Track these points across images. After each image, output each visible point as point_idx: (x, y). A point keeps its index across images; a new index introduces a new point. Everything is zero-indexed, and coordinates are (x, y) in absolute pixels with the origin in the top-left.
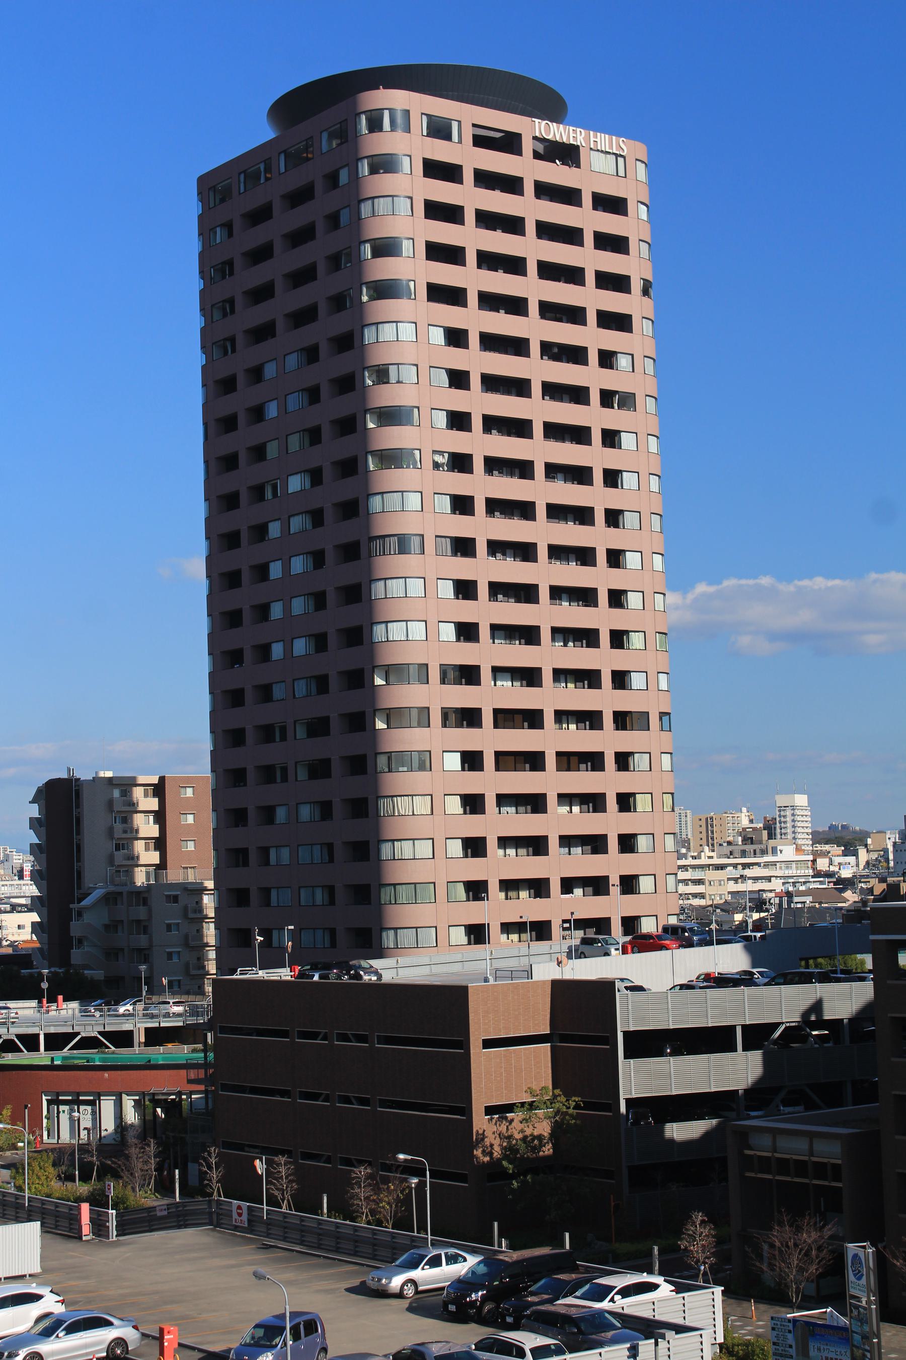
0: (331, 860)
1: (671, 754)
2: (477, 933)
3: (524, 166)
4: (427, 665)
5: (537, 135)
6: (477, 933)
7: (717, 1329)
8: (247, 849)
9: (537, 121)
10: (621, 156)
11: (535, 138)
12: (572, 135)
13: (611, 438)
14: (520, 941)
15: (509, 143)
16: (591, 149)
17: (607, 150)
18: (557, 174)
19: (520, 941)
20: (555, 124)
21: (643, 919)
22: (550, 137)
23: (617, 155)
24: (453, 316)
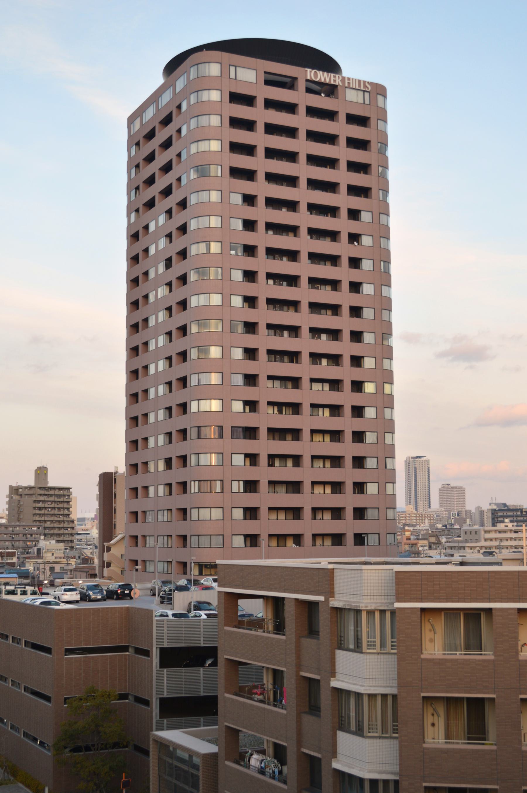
0: (171, 494)
1: (378, 483)
2: (252, 540)
3: (298, 97)
4: (232, 427)
5: (309, 78)
6: (252, 540)
7: (513, 537)
8: (137, 512)
9: (309, 70)
10: (367, 91)
11: (307, 80)
12: (332, 79)
13: (354, 214)
14: (278, 546)
15: (290, 84)
16: (346, 87)
17: (357, 88)
18: (321, 102)
19: (278, 546)
20: (321, 72)
21: (368, 459)
22: (318, 80)
23: (364, 91)
24: (248, 187)
